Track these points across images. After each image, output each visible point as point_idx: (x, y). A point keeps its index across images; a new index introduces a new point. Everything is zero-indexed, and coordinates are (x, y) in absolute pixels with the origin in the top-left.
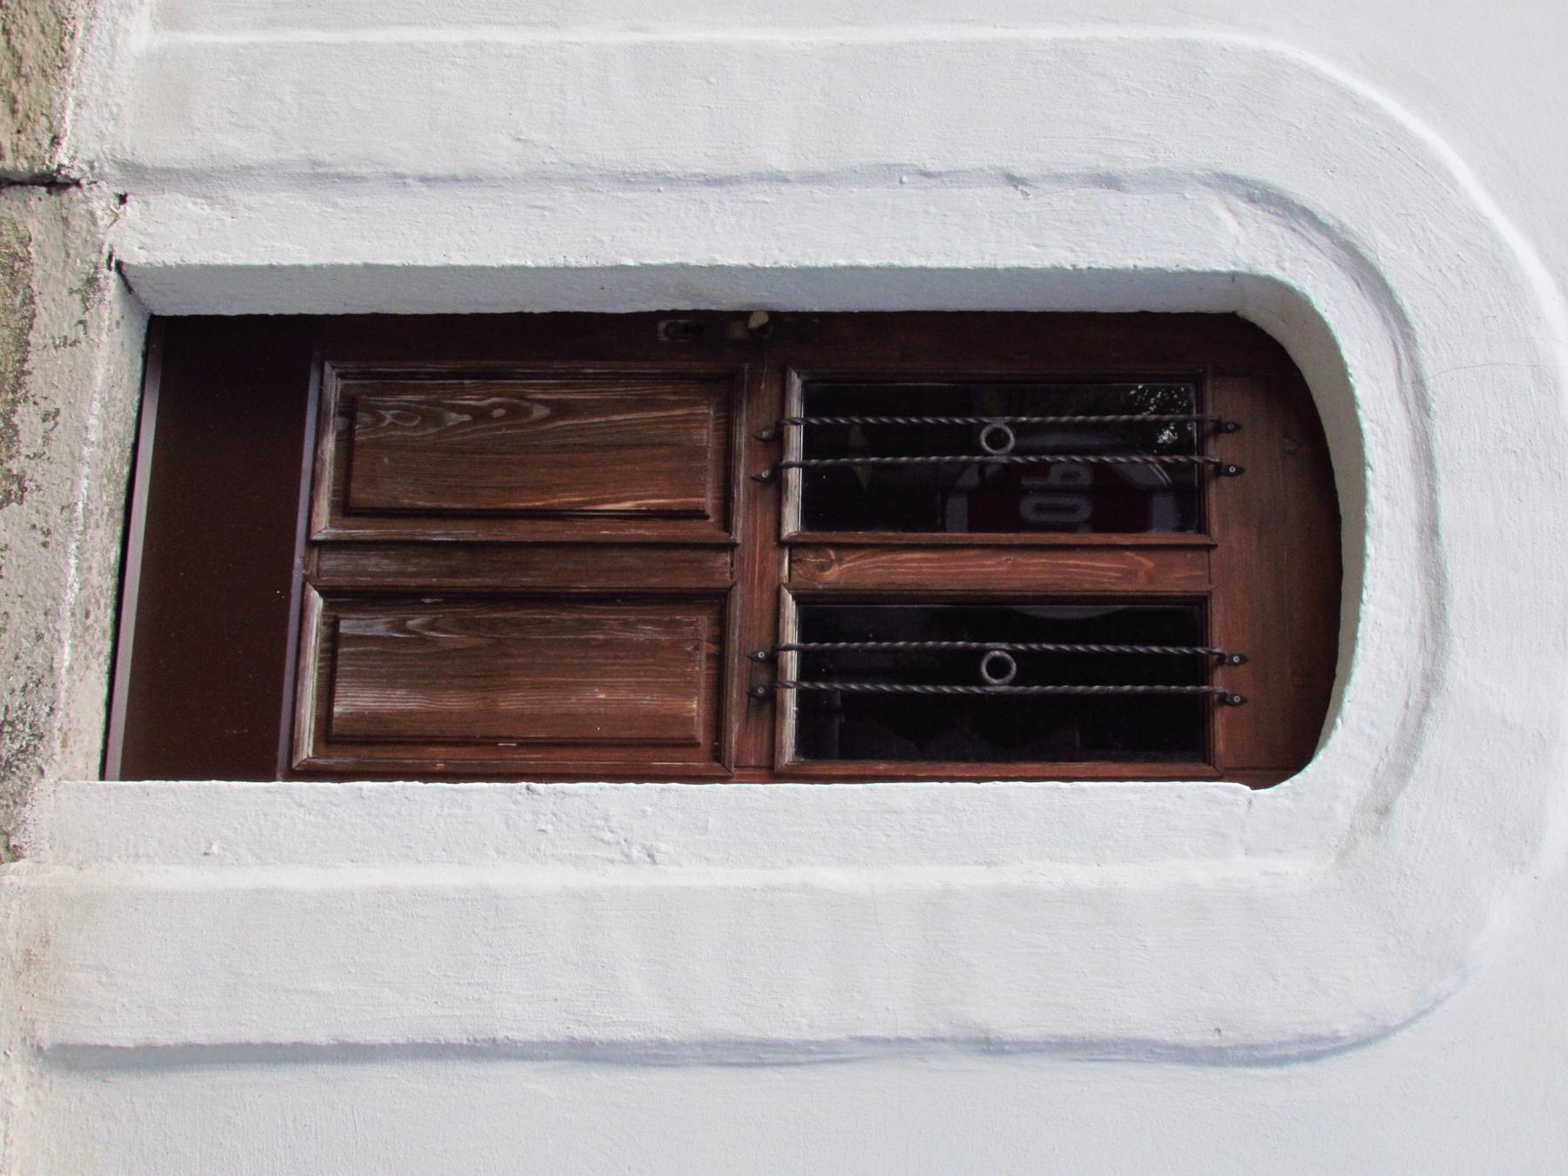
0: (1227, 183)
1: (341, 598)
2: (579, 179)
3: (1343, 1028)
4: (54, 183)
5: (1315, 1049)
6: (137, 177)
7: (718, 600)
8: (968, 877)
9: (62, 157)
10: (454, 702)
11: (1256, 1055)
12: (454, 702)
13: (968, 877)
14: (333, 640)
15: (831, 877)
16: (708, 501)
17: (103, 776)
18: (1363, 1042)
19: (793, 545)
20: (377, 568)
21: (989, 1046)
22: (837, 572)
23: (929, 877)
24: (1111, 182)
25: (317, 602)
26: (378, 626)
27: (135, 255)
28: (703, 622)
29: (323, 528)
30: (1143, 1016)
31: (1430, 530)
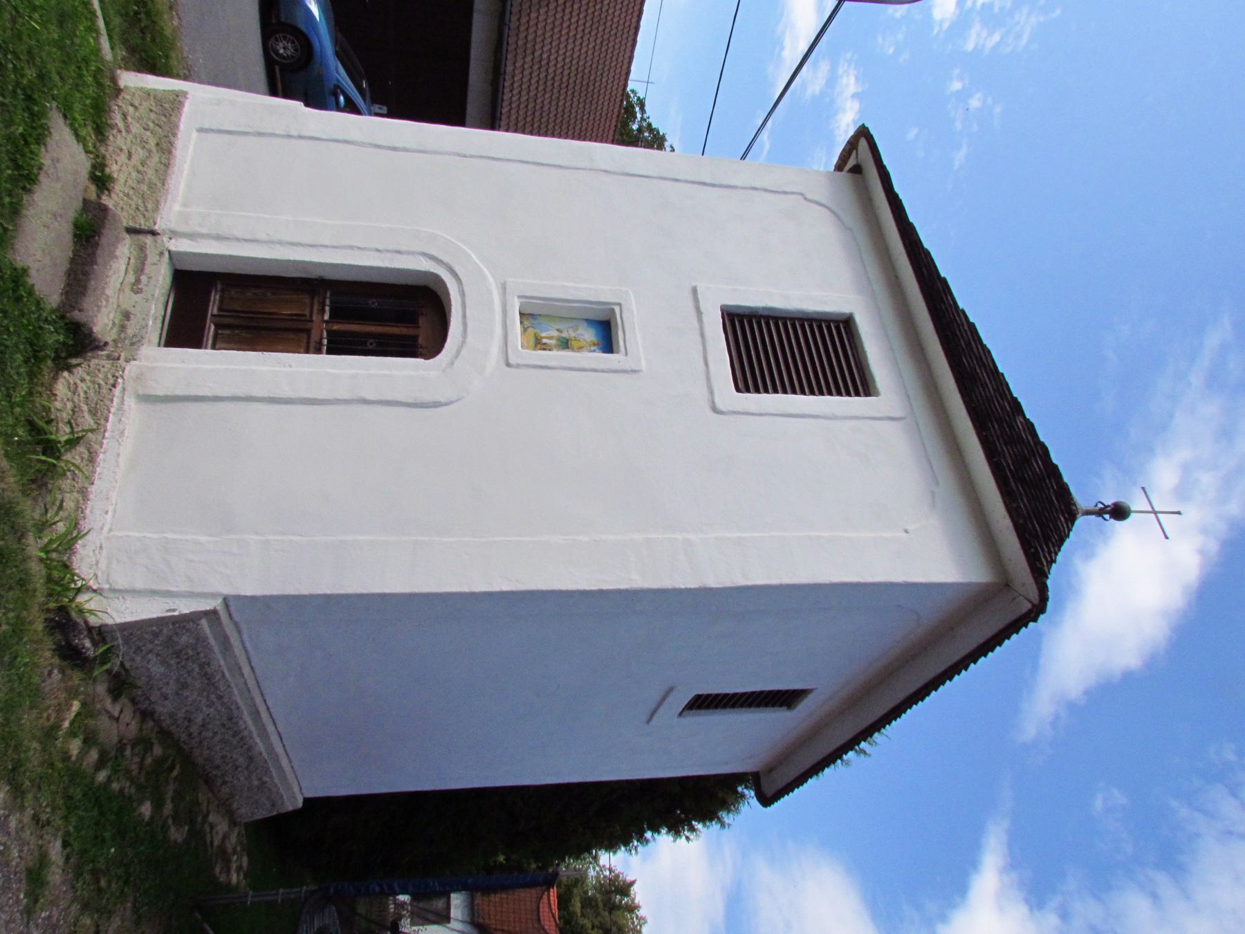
0: (424, 254)
1: (217, 326)
2: (281, 243)
3: (443, 400)
4: (154, 233)
5: (436, 405)
6: (174, 234)
7: (308, 331)
9: (156, 228)
16: (307, 313)
17: (159, 345)
18: (446, 404)
19: (327, 322)
22: (336, 327)
24: (399, 252)
25: (213, 327)
26: (227, 332)
27: (173, 248)
28: (305, 335)
29: (215, 312)
31: (464, 316)
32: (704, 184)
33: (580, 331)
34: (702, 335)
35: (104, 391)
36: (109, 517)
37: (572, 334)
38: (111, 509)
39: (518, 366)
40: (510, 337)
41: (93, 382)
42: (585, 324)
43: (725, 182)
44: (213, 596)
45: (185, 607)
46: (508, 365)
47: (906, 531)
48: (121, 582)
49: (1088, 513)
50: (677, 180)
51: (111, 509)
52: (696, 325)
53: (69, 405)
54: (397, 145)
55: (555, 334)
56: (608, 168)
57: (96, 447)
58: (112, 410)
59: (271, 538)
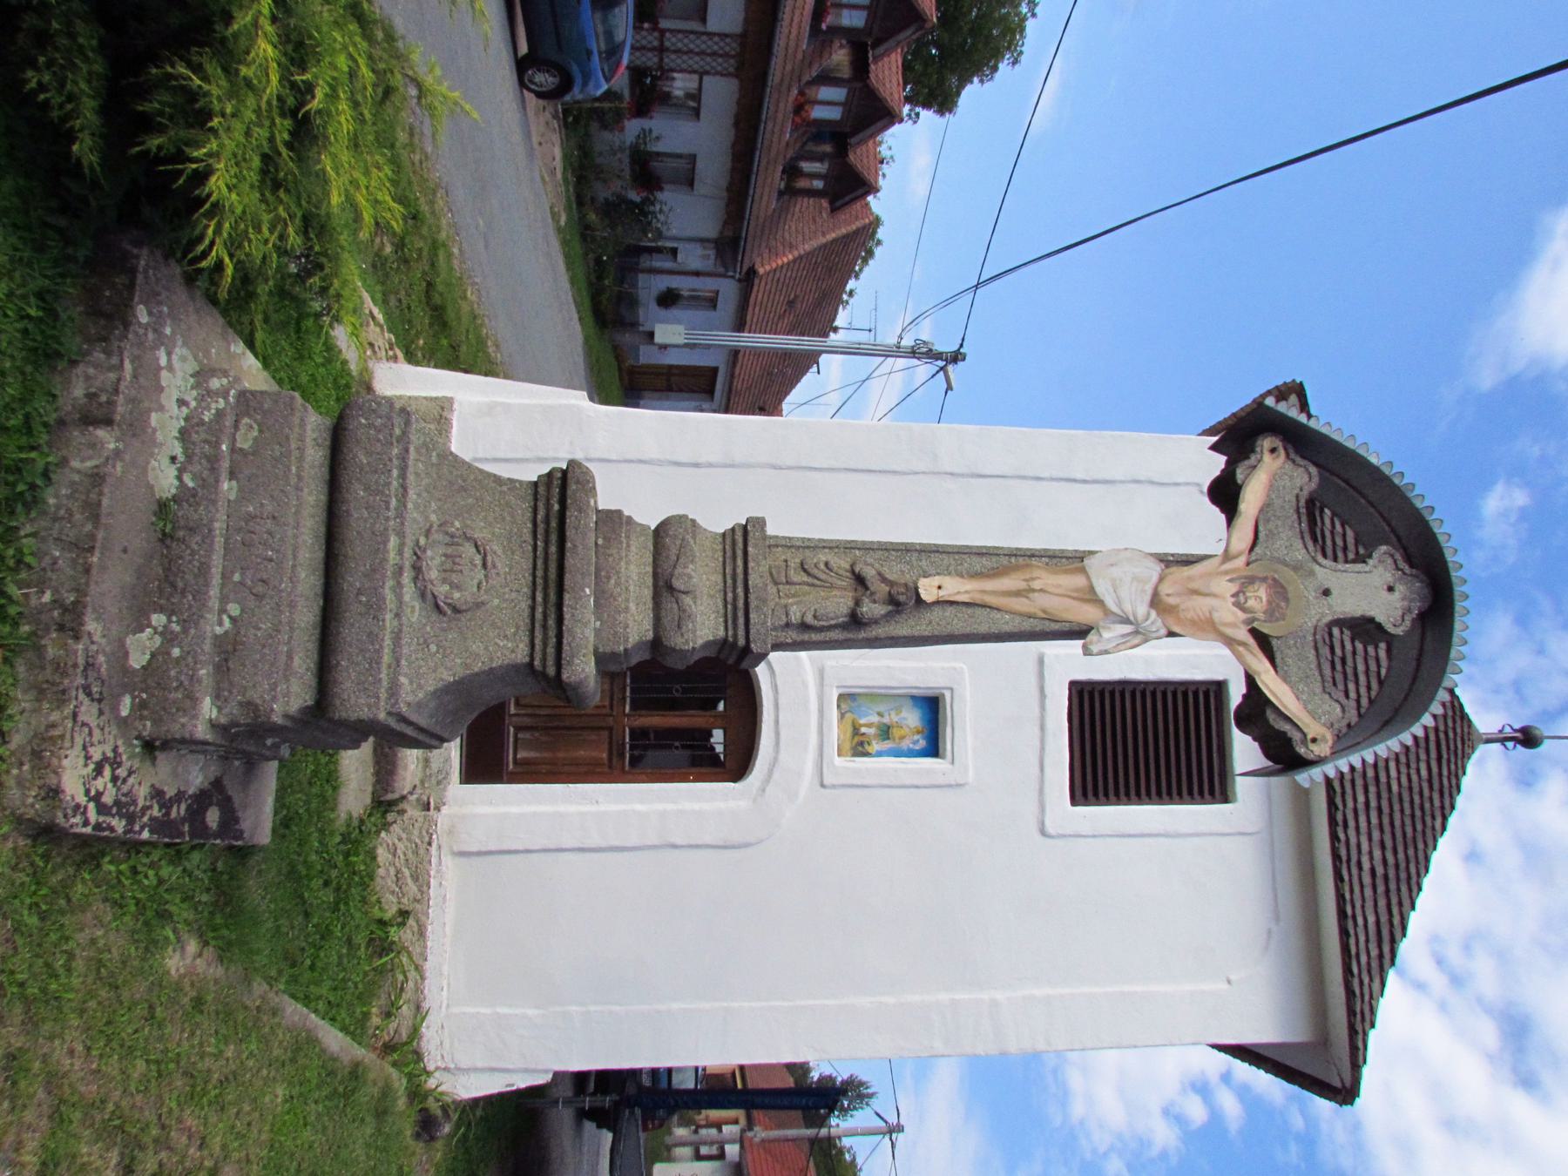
1: (518, 729)
7: (610, 729)
8: (670, 807)
10: (546, 755)
11: (733, 847)
12: (546, 755)
13: (670, 807)
14: (516, 740)
15: (639, 807)
20: (527, 721)
21: (675, 846)
23: (660, 807)
28: (606, 733)
30: (708, 840)
31: (777, 722)
32: (1075, 481)
33: (904, 714)
34: (1042, 728)
35: (422, 852)
36: (445, 993)
37: (895, 718)
38: (445, 983)
39: (834, 787)
40: (825, 749)
41: (409, 840)
42: (910, 702)
43: (1100, 476)
44: (546, 1071)
45: (522, 1082)
46: (823, 786)
47: (1229, 982)
48: (464, 1063)
49: (1488, 741)
50: (1039, 479)
51: (445, 983)
52: (1037, 710)
53: (392, 871)
54: (700, 461)
55: (875, 719)
56: (956, 470)
57: (423, 918)
58: (432, 873)
59: (592, 1008)
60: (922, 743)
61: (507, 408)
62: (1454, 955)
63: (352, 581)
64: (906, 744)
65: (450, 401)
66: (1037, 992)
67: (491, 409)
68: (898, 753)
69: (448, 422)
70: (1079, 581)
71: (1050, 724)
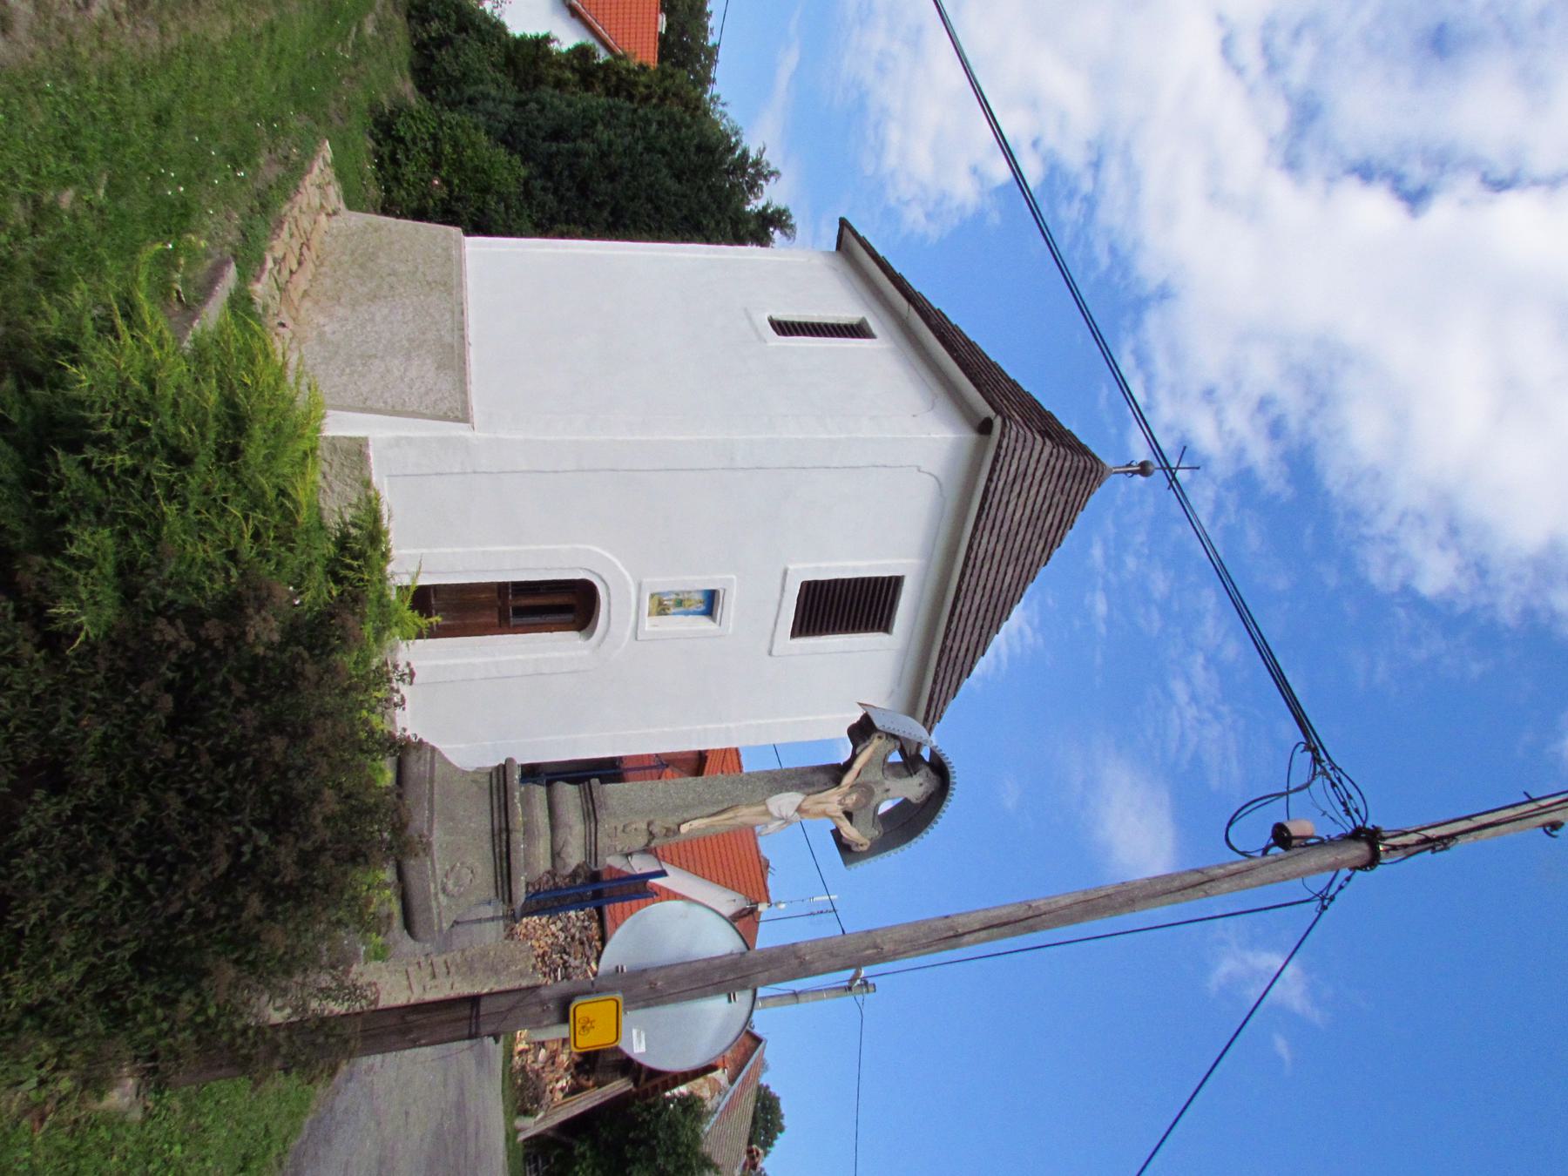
8: (540, 655)
13: (540, 655)
60: (702, 608)
61: (409, 440)
62: (1281, 40)
63: (416, 902)
64: (692, 609)
65: (366, 439)
66: (753, 722)
67: (397, 442)
68: (687, 614)
69: (367, 458)
70: (762, 808)
71: (784, 605)
